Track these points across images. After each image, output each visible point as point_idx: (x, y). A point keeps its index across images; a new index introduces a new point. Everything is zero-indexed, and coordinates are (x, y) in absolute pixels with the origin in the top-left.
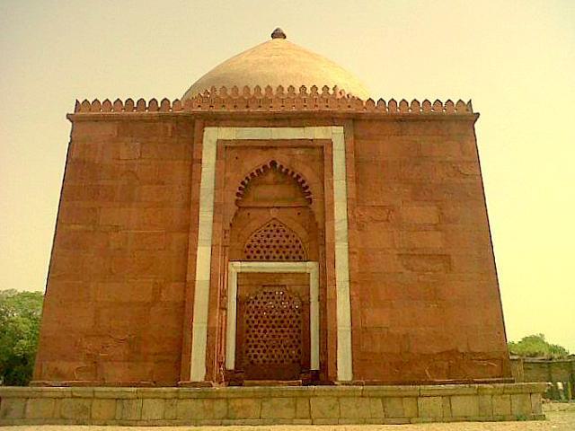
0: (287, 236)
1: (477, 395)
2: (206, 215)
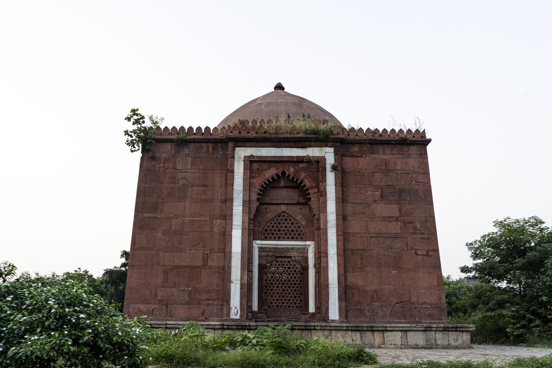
0: (293, 224)
1: (425, 331)
2: (238, 209)
